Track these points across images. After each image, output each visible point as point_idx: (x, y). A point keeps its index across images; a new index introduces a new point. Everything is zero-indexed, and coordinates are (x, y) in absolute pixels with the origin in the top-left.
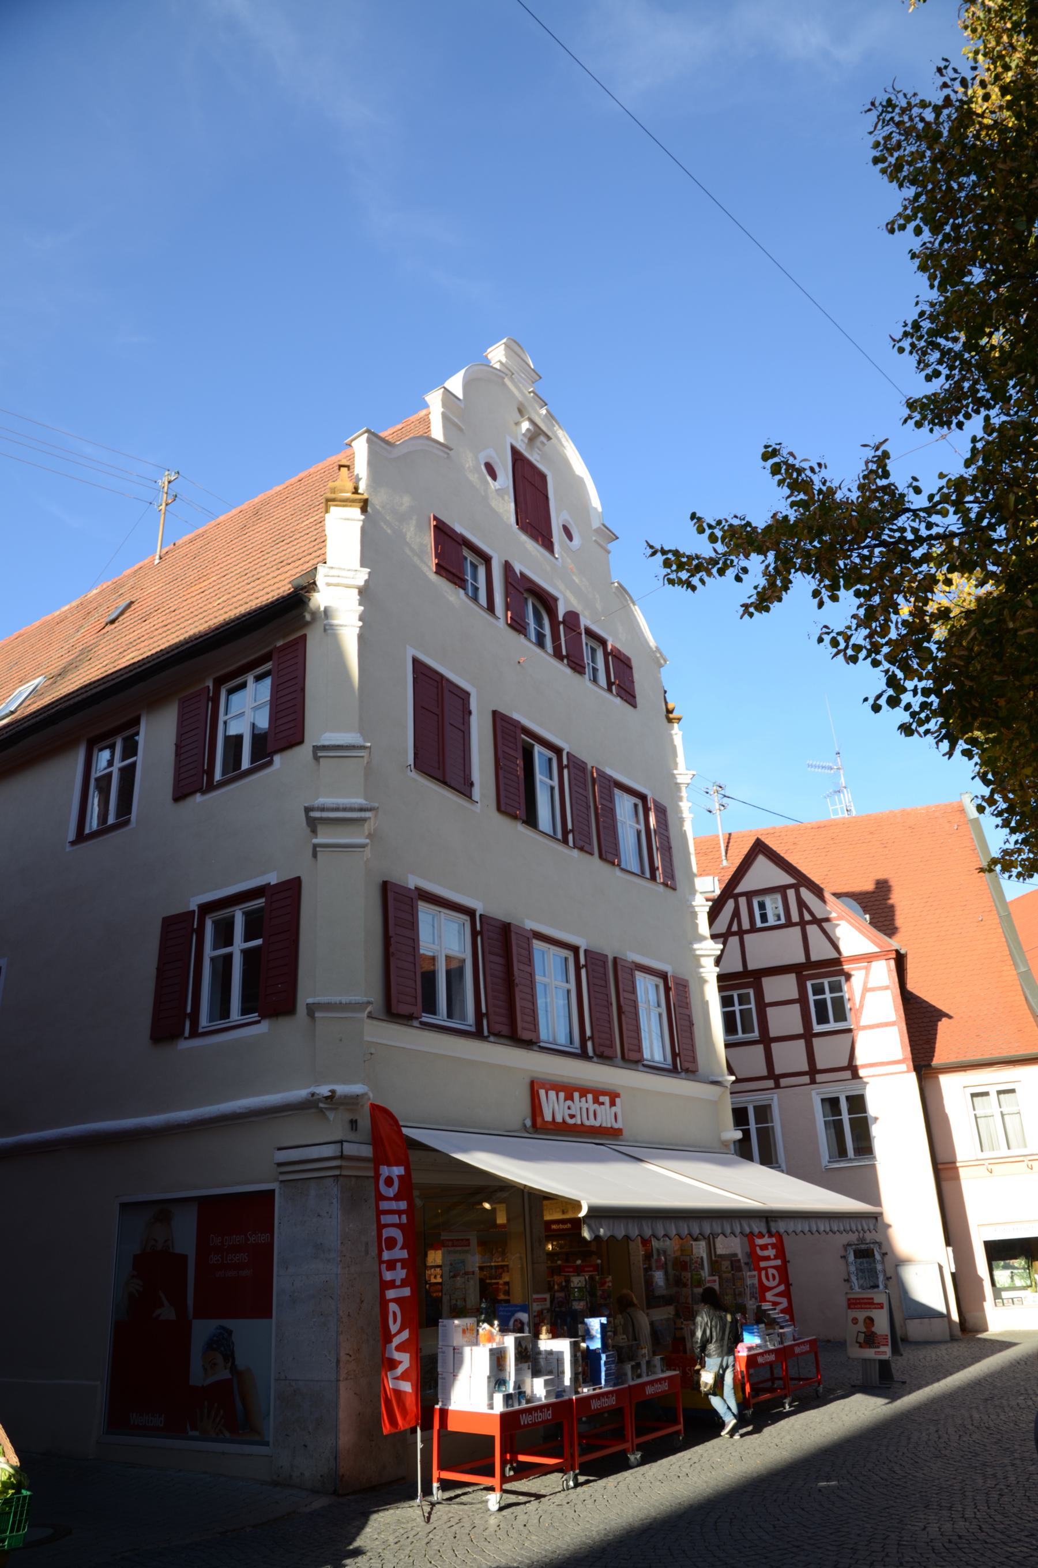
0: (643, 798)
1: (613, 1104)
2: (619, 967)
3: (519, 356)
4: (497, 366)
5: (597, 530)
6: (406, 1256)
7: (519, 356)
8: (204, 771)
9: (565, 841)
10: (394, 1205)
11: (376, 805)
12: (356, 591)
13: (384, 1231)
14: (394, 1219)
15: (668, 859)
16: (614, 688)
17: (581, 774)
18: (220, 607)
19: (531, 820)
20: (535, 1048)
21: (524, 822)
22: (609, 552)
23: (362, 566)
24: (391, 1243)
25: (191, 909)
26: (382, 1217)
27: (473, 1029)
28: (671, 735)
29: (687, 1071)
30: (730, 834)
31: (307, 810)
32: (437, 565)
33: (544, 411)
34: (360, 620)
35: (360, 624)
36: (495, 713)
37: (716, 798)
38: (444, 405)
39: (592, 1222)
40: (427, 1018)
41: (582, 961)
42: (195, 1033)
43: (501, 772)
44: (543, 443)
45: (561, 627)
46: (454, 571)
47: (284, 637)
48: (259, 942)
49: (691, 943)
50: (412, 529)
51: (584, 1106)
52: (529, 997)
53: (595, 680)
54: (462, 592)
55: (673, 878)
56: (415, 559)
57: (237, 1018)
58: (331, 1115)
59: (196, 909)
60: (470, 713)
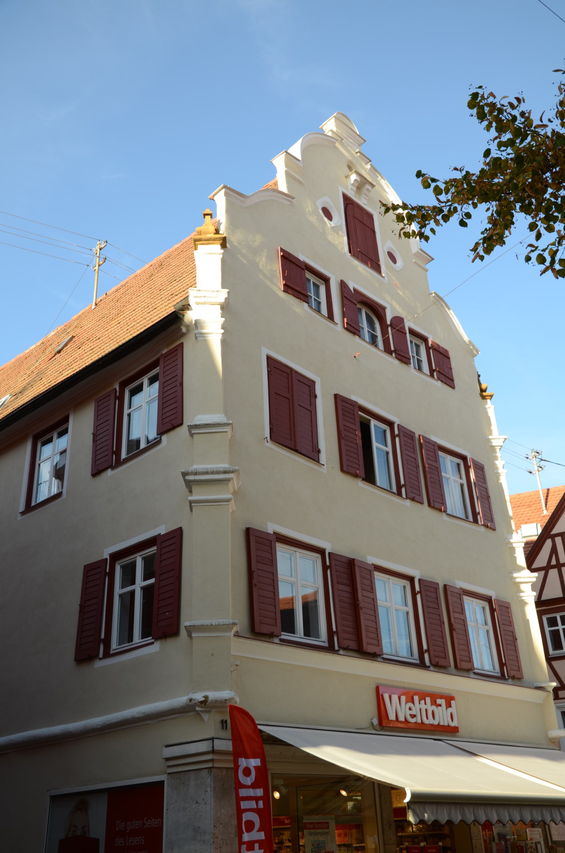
0: (464, 458)
1: (449, 705)
2: (449, 593)
3: (347, 126)
4: (330, 134)
5: (415, 254)
6: (263, 838)
7: (347, 126)
8: (113, 452)
9: (399, 494)
10: (251, 792)
11: (237, 468)
12: (220, 306)
13: (244, 815)
14: (252, 804)
15: (487, 506)
16: (435, 373)
17: (411, 441)
18: (128, 331)
19: (369, 477)
20: (379, 659)
21: (363, 479)
22: (427, 271)
23: (223, 287)
24: (250, 826)
25: (104, 557)
26: (242, 803)
27: (326, 645)
28: (485, 409)
29: (513, 678)
30: (548, 490)
31: (184, 474)
32: (285, 285)
33: (369, 166)
34: (223, 328)
35: (223, 331)
36: (336, 396)
37: (535, 461)
38: (287, 165)
39: (417, 807)
40: (285, 636)
41: (417, 588)
42: (107, 655)
43: (343, 442)
44: (368, 190)
45: (390, 329)
46: (299, 289)
47: (168, 346)
48: (152, 581)
49: (511, 573)
50: (263, 259)
51: (423, 707)
52: (373, 618)
53: (420, 369)
54: (306, 305)
55: (492, 520)
56: (267, 281)
57: (138, 641)
58: (205, 717)
59: (108, 557)
60: (316, 397)
